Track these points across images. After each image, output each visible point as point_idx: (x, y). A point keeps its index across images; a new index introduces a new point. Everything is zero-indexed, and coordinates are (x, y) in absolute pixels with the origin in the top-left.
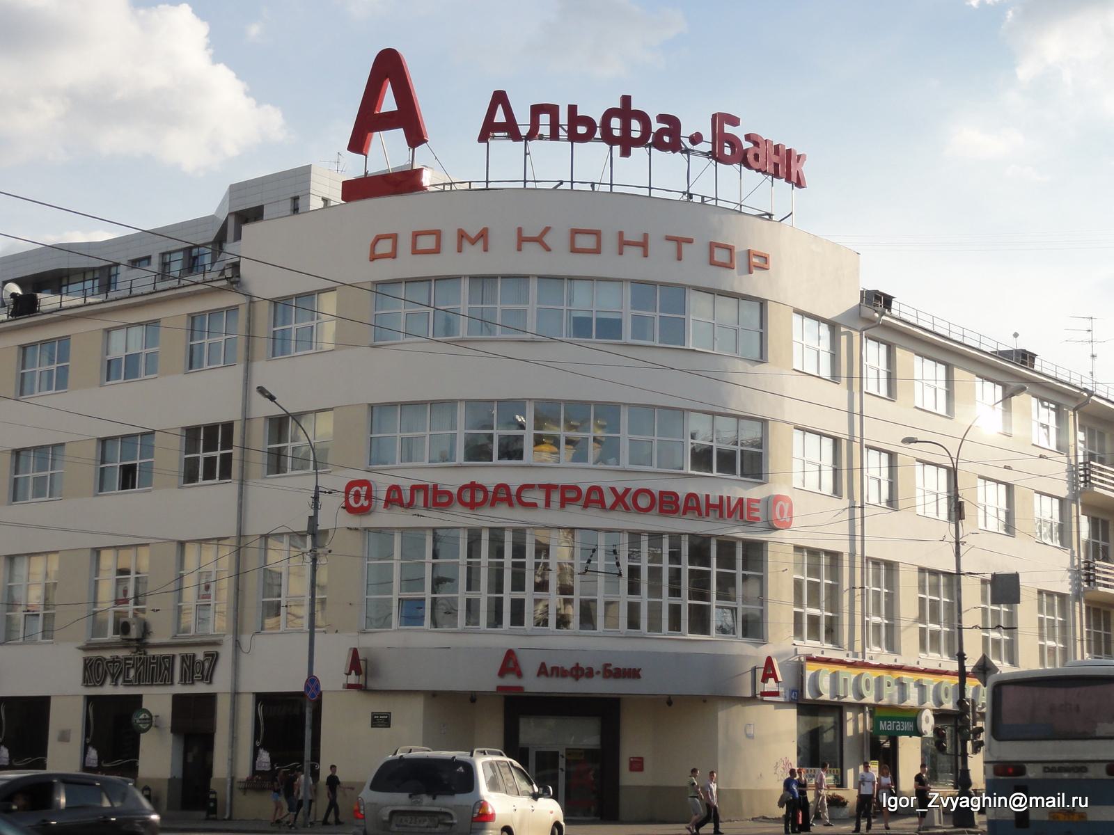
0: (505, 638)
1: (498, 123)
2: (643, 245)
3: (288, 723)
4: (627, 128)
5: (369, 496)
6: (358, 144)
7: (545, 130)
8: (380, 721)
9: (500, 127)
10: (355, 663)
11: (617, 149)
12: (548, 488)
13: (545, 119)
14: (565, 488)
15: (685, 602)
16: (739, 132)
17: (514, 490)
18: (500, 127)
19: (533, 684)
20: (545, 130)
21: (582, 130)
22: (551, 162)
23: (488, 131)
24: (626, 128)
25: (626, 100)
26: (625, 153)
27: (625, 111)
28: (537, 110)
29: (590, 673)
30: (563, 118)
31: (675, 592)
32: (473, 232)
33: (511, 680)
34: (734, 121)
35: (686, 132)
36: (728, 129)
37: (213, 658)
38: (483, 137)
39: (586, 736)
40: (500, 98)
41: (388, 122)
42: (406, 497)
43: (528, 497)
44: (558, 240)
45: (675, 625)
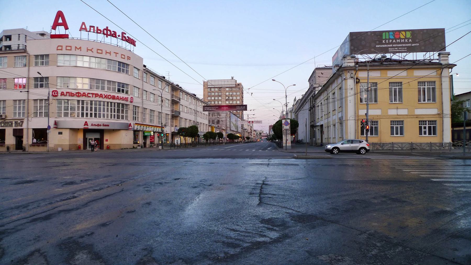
0: (84, 119)
1: (83, 28)
2: (110, 53)
3: (41, 135)
4: (107, 32)
5: (57, 93)
6: (54, 28)
7: (92, 30)
8: (60, 133)
9: (84, 29)
10: (56, 123)
11: (105, 36)
12: (93, 94)
13: (92, 28)
14: (96, 94)
15: (116, 114)
16: (126, 36)
17: (86, 94)
18: (84, 29)
19: (90, 127)
20: (92, 30)
21: (99, 31)
22: (93, 36)
23: (81, 29)
24: (107, 32)
25: (107, 27)
26: (107, 37)
27: (107, 29)
28: (91, 27)
29: (100, 125)
30: (96, 29)
31: (114, 112)
32: (78, 47)
33: (86, 126)
34: (125, 34)
35: (117, 35)
36: (124, 35)
37: (22, 122)
38: (80, 30)
39: (98, 136)
40: (83, 23)
41: (60, 25)
42: (65, 94)
43: (89, 95)
44: (95, 50)
45: (114, 117)
